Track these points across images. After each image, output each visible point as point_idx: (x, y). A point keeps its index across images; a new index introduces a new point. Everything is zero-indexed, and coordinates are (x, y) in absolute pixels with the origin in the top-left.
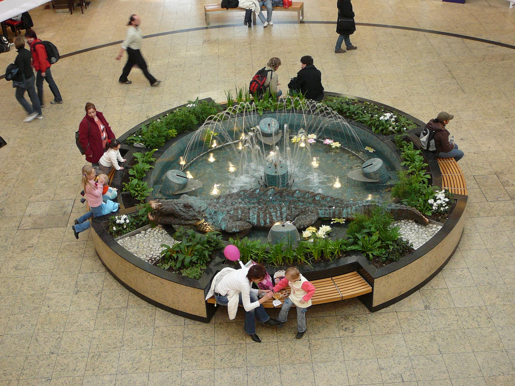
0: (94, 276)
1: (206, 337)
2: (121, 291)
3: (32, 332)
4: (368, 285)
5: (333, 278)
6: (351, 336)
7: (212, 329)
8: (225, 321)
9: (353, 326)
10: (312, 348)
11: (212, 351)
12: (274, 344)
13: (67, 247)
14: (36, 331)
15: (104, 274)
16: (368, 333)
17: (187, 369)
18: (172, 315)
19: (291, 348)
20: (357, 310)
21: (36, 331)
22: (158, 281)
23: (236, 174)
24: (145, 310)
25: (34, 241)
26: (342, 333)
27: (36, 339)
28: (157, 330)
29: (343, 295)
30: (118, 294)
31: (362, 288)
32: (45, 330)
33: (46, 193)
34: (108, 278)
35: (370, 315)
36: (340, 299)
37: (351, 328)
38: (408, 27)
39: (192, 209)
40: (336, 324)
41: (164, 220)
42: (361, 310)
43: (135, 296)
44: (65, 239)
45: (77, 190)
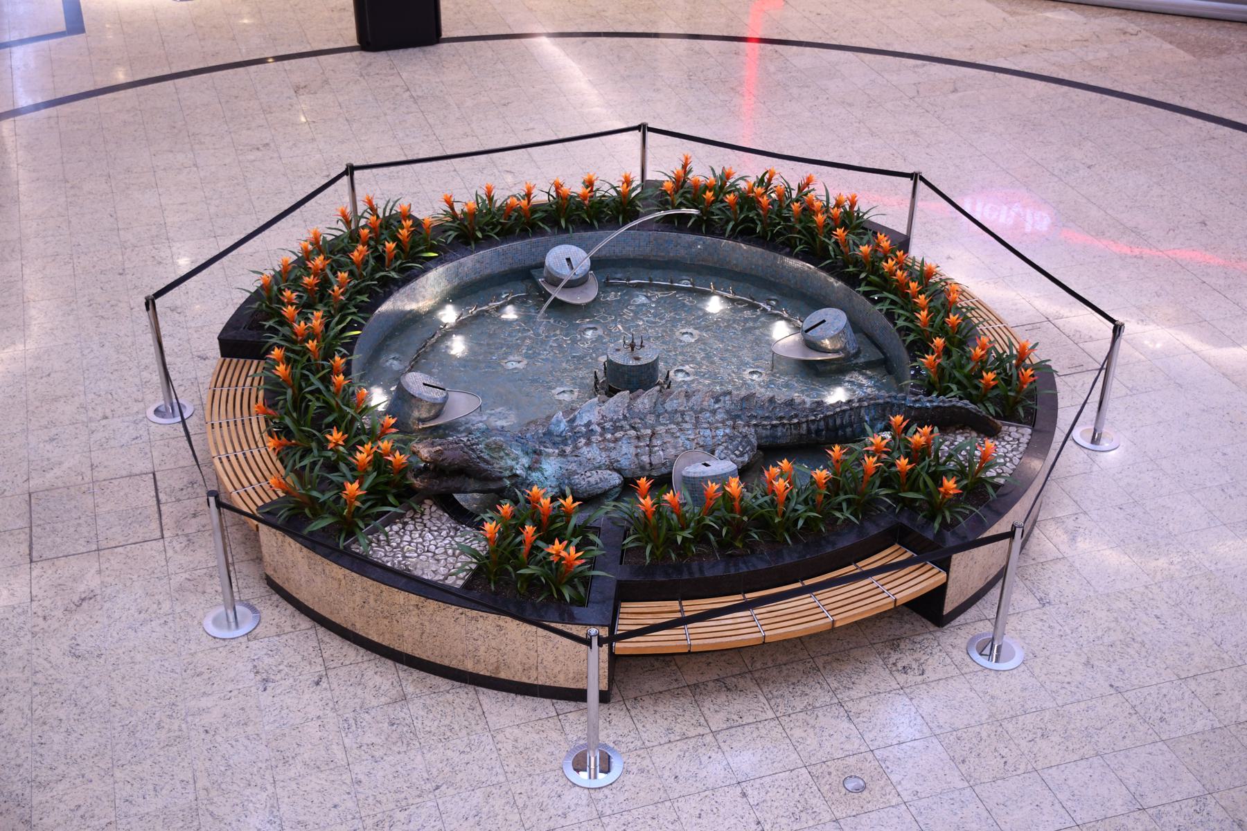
0: (291, 642)
1: (620, 732)
2: (372, 663)
3: (191, 797)
4: (936, 570)
5: (684, 603)
6: (923, 682)
7: (622, 713)
8: (644, 693)
9: (916, 660)
10: (856, 721)
11: (647, 762)
12: (772, 724)
13: (187, 585)
14: (202, 794)
15: (311, 632)
16: (952, 670)
17: (609, 812)
18: (519, 698)
19: (813, 727)
20: (908, 626)
21: (202, 794)
22: (489, 622)
23: (705, 323)
24: (450, 697)
25: (92, 581)
26: (901, 678)
27: (212, 814)
28: (500, 737)
29: (693, 642)
30: (370, 673)
31: (917, 582)
32: (223, 786)
33: (66, 465)
34: (327, 639)
35: (938, 634)
36: (892, 606)
37: (915, 665)
38: (816, 50)
39: (502, 454)
40: (881, 662)
41: (444, 484)
42: (920, 623)
43: (413, 670)
44: (172, 568)
45: (147, 450)
